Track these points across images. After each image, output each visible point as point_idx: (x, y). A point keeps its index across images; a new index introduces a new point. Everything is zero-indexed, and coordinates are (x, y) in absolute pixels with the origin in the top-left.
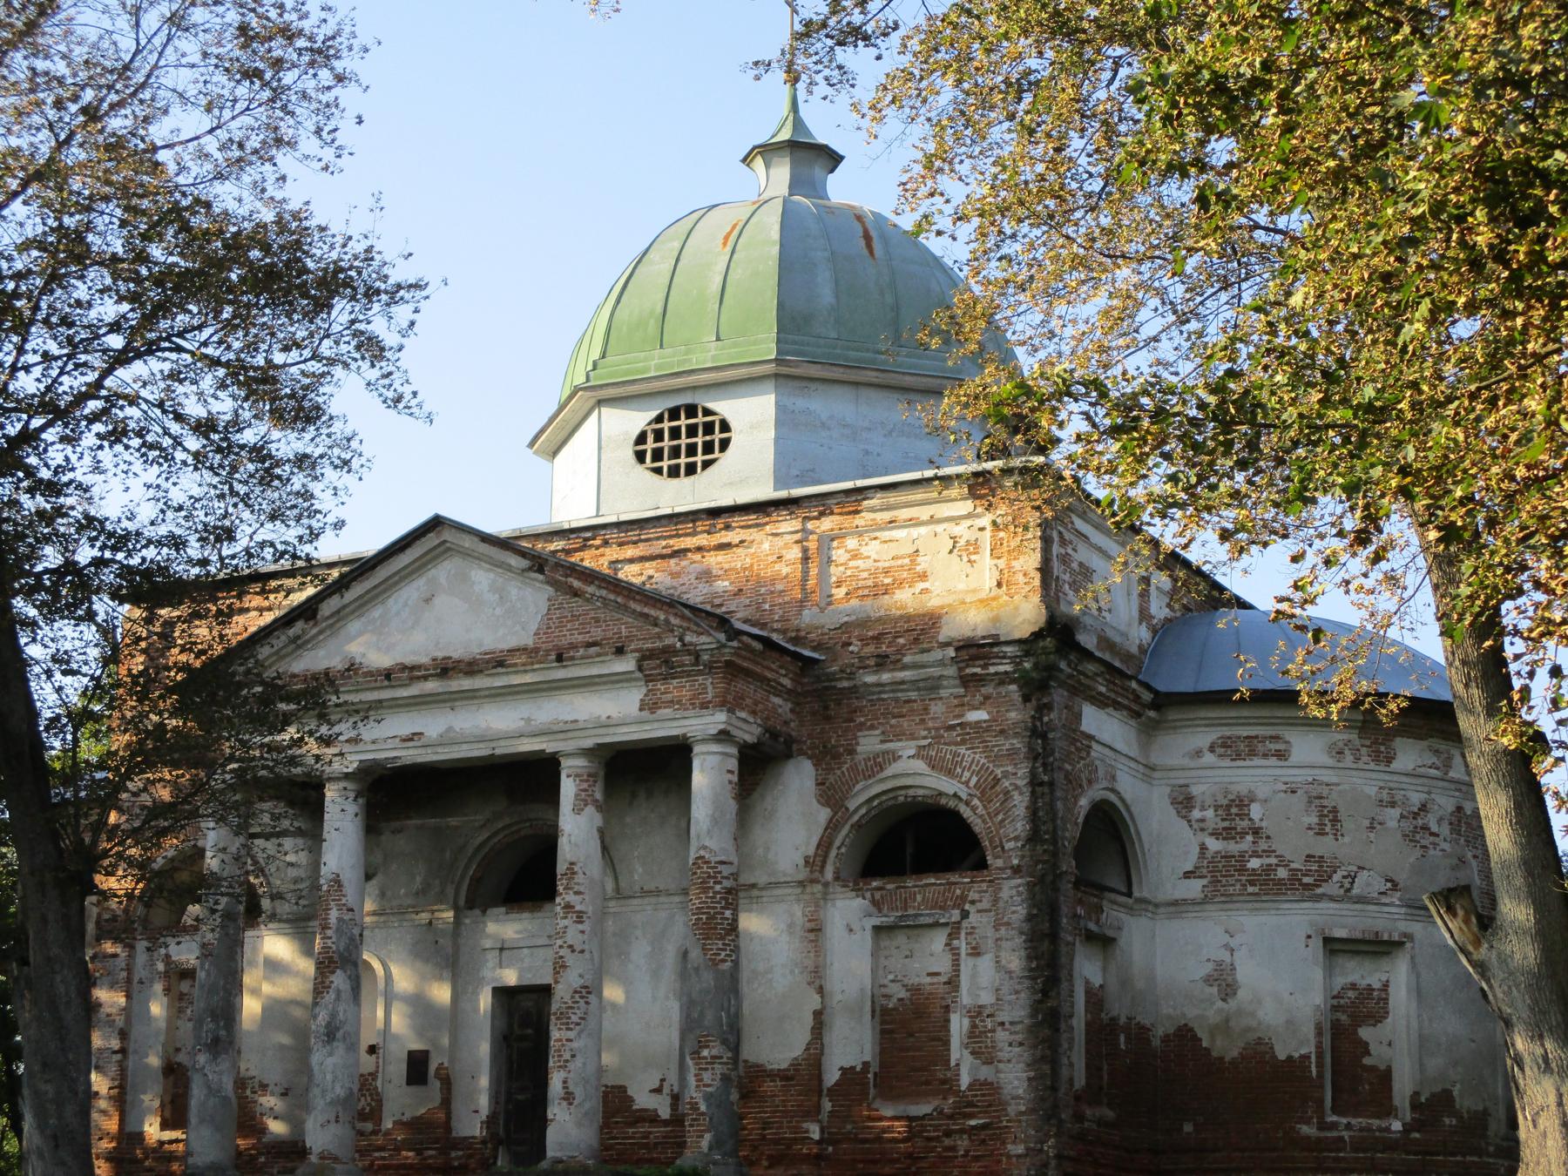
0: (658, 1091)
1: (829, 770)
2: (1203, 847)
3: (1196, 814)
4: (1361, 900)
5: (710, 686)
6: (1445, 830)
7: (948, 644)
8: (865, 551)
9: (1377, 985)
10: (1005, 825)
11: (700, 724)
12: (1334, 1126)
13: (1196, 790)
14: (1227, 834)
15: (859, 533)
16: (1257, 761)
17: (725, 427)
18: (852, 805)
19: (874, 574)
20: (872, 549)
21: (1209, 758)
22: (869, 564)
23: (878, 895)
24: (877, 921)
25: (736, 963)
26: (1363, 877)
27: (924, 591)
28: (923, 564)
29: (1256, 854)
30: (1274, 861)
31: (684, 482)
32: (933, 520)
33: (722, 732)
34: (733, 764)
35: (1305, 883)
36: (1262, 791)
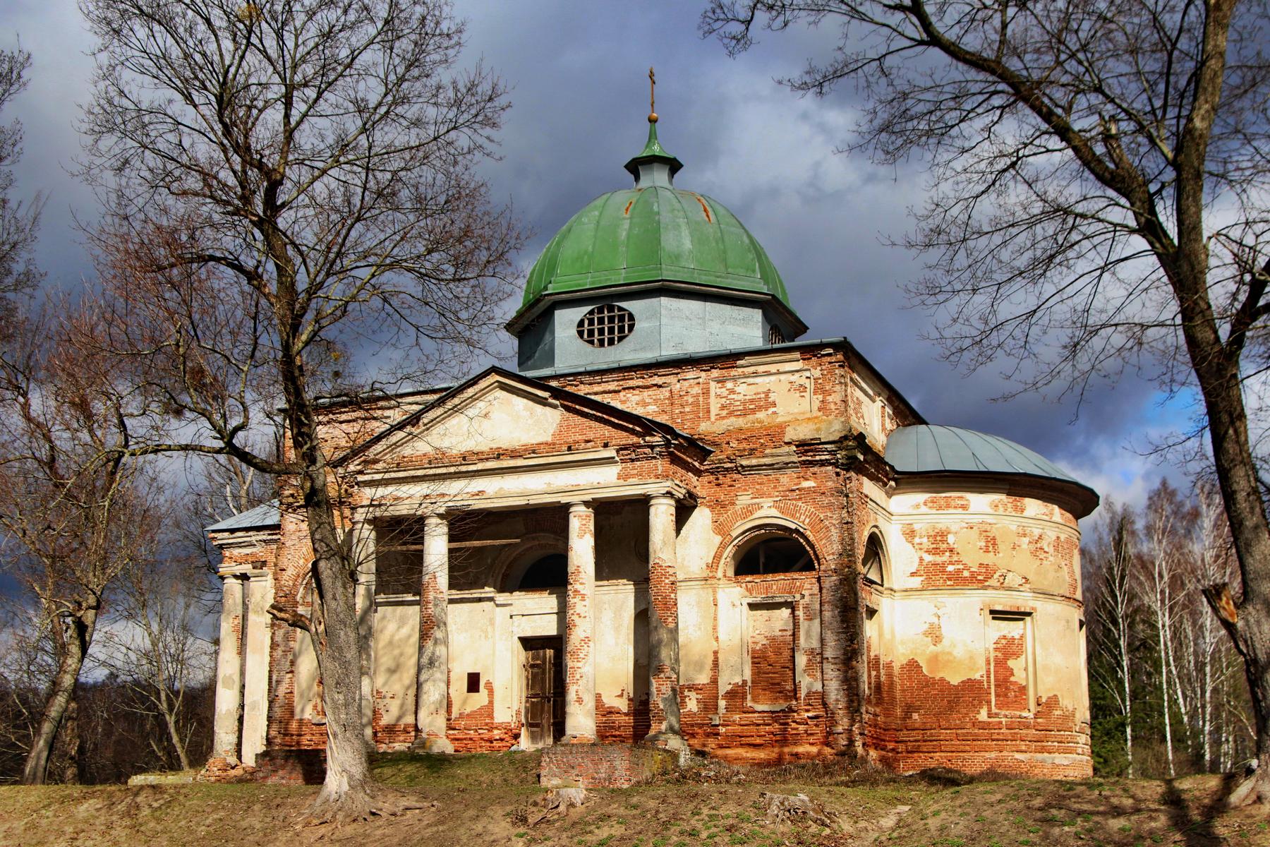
0: (621, 696)
1: (719, 514)
2: (921, 559)
3: (917, 540)
4: (1010, 589)
5: (661, 465)
6: (1051, 550)
7: (788, 444)
8: (738, 389)
9: (1017, 637)
10: (828, 548)
11: (651, 488)
12: (997, 715)
13: (916, 527)
14: (935, 551)
15: (734, 379)
16: (951, 511)
17: (631, 317)
18: (734, 534)
19: (744, 403)
20: (742, 388)
21: (924, 509)
22: (740, 397)
23: (749, 585)
24: (751, 600)
25: (677, 624)
26: (1010, 575)
27: (774, 413)
28: (772, 397)
29: (951, 563)
30: (961, 567)
31: (607, 349)
32: (779, 373)
33: (668, 493)
34: (673, 510)
35: (979, 579)
36: (953, 529)
